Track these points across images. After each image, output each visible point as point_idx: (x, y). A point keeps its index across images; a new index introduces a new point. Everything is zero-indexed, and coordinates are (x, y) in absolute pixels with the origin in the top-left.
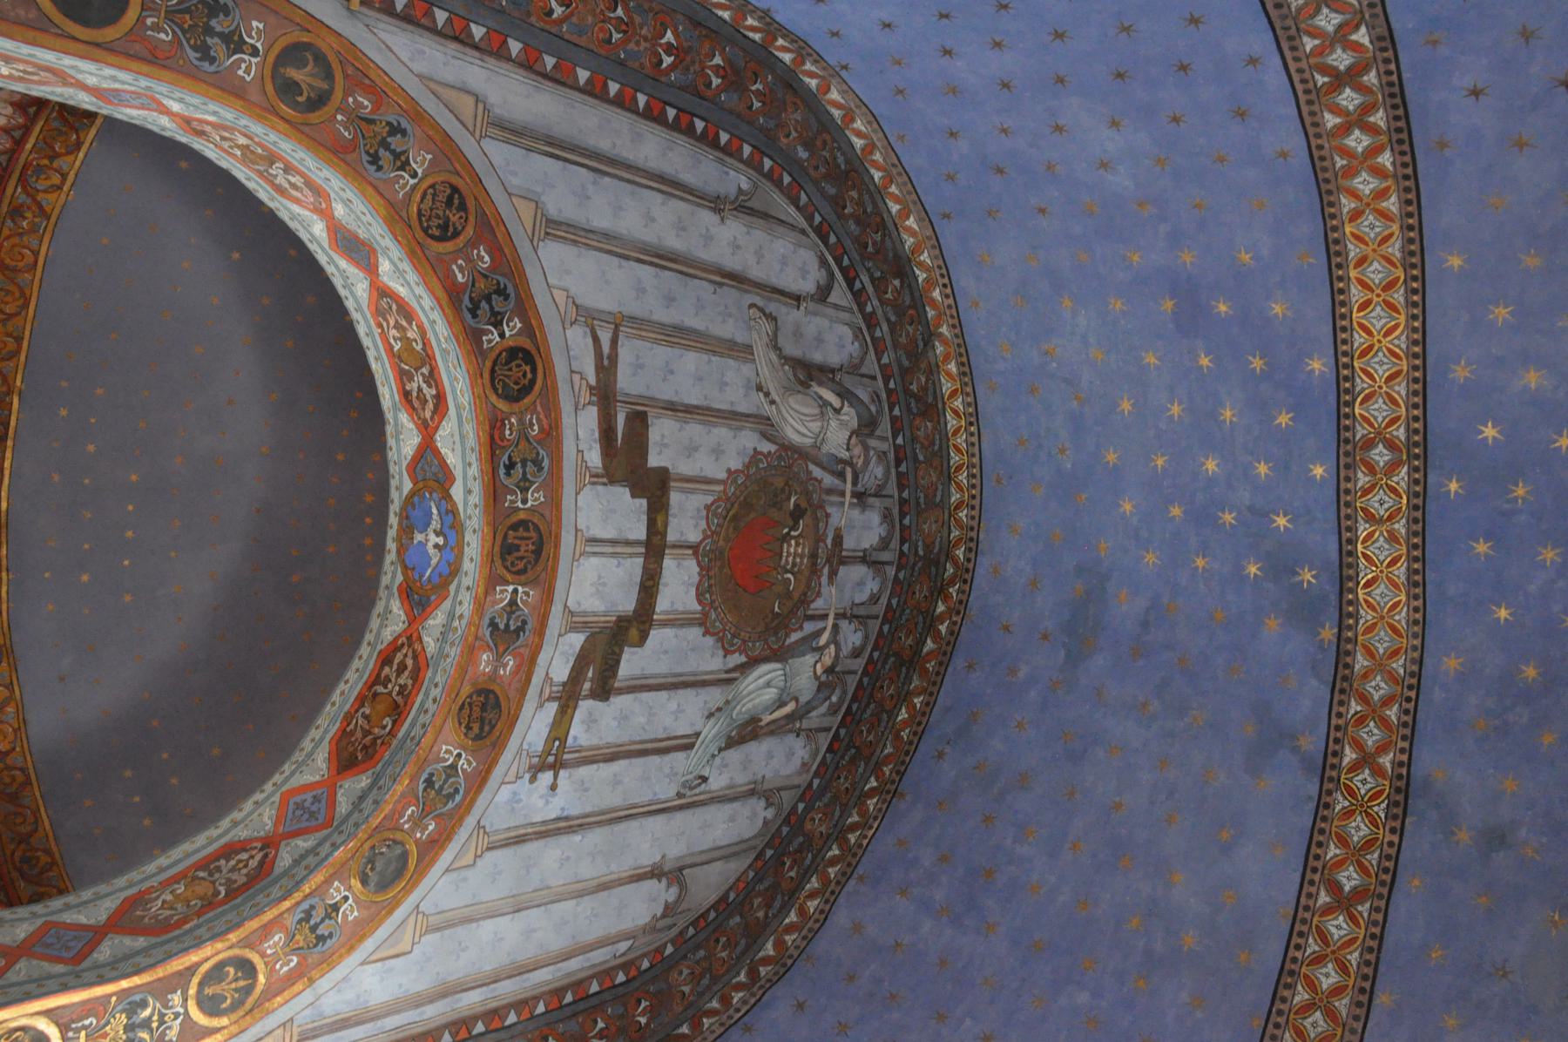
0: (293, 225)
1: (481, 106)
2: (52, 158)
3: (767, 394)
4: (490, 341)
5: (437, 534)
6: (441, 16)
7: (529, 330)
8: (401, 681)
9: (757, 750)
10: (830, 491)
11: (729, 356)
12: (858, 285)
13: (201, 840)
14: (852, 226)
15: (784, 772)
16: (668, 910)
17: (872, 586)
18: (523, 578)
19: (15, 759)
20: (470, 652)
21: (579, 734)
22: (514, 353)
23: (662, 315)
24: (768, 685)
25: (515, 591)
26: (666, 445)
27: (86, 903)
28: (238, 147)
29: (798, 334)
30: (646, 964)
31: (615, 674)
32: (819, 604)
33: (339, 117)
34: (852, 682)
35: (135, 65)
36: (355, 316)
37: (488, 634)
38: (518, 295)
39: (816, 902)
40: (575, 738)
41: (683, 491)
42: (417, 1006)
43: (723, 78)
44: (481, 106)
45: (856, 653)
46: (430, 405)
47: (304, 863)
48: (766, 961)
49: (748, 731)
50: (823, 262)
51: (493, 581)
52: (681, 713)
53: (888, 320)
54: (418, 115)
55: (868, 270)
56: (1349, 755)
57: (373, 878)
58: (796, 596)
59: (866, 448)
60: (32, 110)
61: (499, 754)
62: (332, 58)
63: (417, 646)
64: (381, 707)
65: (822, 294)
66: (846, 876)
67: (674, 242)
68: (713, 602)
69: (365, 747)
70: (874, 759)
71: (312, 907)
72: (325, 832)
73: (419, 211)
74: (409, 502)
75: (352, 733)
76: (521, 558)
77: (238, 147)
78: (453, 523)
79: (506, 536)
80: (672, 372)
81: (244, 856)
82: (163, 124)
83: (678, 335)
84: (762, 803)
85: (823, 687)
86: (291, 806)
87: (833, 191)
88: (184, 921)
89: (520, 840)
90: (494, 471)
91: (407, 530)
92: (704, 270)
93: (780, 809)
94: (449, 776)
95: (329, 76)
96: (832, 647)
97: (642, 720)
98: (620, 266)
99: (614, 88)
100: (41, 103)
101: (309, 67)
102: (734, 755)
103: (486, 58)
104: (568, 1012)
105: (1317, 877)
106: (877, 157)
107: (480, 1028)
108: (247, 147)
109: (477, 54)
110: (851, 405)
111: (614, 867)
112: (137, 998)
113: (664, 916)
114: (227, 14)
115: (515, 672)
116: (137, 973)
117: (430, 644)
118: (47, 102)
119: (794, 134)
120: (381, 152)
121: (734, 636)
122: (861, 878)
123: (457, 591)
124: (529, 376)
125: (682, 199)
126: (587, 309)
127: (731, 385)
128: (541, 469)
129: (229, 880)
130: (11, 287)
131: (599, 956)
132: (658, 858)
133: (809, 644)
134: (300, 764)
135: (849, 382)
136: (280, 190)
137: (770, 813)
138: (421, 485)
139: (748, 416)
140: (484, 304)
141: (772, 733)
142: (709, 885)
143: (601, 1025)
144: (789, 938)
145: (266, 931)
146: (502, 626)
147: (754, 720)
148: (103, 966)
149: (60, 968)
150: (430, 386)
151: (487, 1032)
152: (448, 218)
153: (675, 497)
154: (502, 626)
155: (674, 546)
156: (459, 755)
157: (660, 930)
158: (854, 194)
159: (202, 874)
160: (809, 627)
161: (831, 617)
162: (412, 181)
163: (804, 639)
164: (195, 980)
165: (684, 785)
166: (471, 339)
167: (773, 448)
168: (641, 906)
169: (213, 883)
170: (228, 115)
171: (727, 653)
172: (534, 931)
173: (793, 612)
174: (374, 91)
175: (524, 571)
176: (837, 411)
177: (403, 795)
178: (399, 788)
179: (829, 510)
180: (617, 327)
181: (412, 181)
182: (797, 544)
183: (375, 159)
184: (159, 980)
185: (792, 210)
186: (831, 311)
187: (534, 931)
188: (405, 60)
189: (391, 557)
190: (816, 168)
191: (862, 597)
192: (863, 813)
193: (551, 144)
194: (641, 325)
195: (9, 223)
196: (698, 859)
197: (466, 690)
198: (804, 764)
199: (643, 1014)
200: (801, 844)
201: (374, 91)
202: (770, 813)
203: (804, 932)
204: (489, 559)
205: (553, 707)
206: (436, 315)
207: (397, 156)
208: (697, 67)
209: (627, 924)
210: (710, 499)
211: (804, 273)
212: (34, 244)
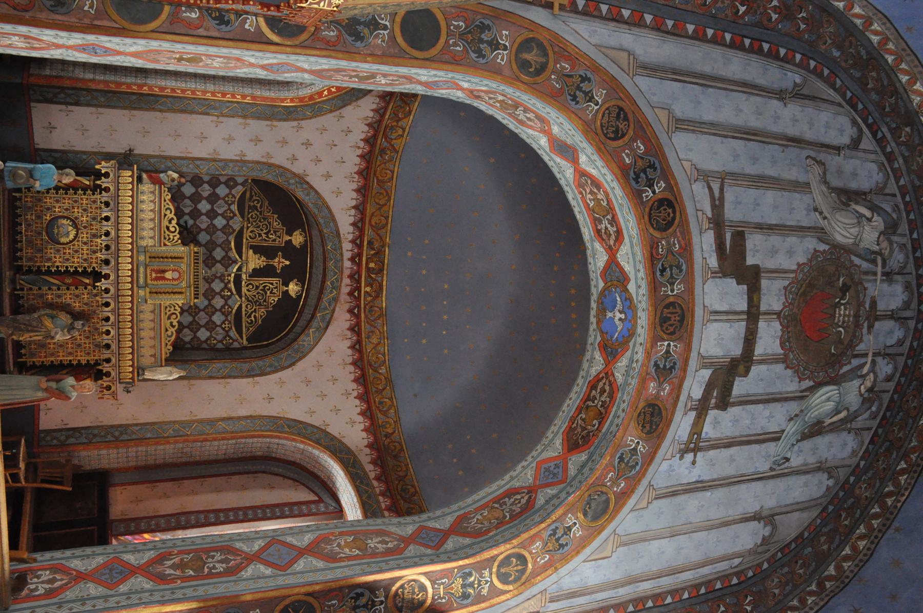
0: (528, 141)
1: (632, 57)
2: (397, 121)
3: (821, 213)
4: (647, 196)
5: (621, 312)
6: (604, 8)
8: (603, 399)
9: (821, 441)
10: (867, 273)
11: (795, 191)
12: (880, 135)
13: (494, 486)
14: (874, 96)
15: (840, 456)
16: (765, 541)
17: (899, 334)
18: (673, 337)
19: (396, 437)
20: (643, 383)
21: (708, 430)
22: (662, 202)
23: (751, 170)
24: (828, 400)
25: (669, 345)
26: (757, 251)
27: (439, 517)
28: (498, 101)
29: (840, 172)
30: (750, 574)
31: (730, 395)
32: (861, 347)
33: (553, 77)
34: (886, 398)
35: (445, 67)
36: (566, 189)
37: (653, 371)
38: (662, 168)
39: (864, 542)
40: (707, 433)
41: (769, 278)
42: (615, 588)
43: (779, 14)
44: (632, 57)
45: (889, 379)
46: (613, 237)
47: (552, 502)
48: (830, 578)
49: (816, 429)
50: (854, 123)
53: (903, 155)
54: (596, 68)
55: (887, 124)
58: (846, 342)
59: (891, 243)
60: (388, 98)
61: (661, 442)
62: (546, 44)
63: (611, 378)
64: (591, 414)
65: (855, 144)
66: (885, 527)
67: (754, 123)
68: (791, 347)
69: (583, 437)
70: (903, 450)
71: (557, 528)
72: (562, 486)
73: (601, 124)
74: (602, 294)
75: (575, 429)
76: (671, 325)
77: (498, 101)
78: (630, 306)
79: (662, 311)
80: (758, 205)
81: (518, 497)
82: (458, 95)
83: (761, 181)
84: (826, 476)
85: (866, 401)
86: (543, 470)
87: (858, 75)
88: (489, 531)
89: (674, 494)
90: (654, 273)
91: (602, 311)
92: (775, 138)
94: (633, 455)
95: (546, 55)
96: (872, 375)
97: (748, 422)
98: (722, 143)
99: (710, 32)
100: (392, 94)
101: (535, 51)
102: (807, 445)
103: (632, 28)
104: (703, 599)
106: (891, 46)
107: (650, 604)
108: (503, 101)
109: (627, 27)
110: (879, 215)
111: (731, 512)
112: (467, 571)
113: (761, 545)
114: (489, 30)
115: (670, 393)
116: (467, 558)
117: (619, 377)
118: (395, 92)
119: (829, 41)
120: (578, 93)
121: (805, 369)
122: (897, 530)
123: (634, 345)
124: (672, 215)
125: (757, 95)
126: (704, 171)
127: (796, 209)
128: (681, 271)
129: (511, 509)
130: (382, 191)
131: (722, 566)
132: (758, 508)
133: (855, 373)
134: (546, 446)
135: (877, 200)
136: (521, 122)
137: (831, 482)
138: (609, 284)
139: (809, 228)
140: (642, 175)
141: (831, 431)
142: (792, 526)
144: (846, 565)
145: (532, 539)
146: (661, 366)
147: (819, 422)
148: (451, 552)
149: (429, 551)
150: (612, 226)
151: (654, 607)
152: (618, 126)
153: (764, 283)
154: (661, 366)
155: (765, 314)
156: (638, 443)
157: (760, 553)
158: (874, 74)
159: (496, 505)
160: (855, 362)
161: (870, 355)
162: (596, 108)
163: (852, 370)
164: (496, 564)
165: (774, 463)
166: (636, 196)
167: (827, 247)
168: (747, 537)
169: (503, 510)
170: (494, 85)
171: (801, 380)
172: (682, 548)
173: (843, 354)
174: (569, 58)
175: (673, 333)
178: (605, 461)
179: (866, 285)
180: (723, 179)
181: (596, 108)
182: (845, 309)
183: (574, 98)
184: (478, 562)
185: (831, 92)
186: (861, 154)
187: (682, 548)
188: (586, 37)
189: (593, 326)
190: (846, 61)
192: (897, 484)
193: (674, 73)
194: (736, 177)
195: (379, 158)
196: (784, 510)
197: (642, 404)
198: (853, 451)
199: (748, 604)
200: (853, 503)
202: (831, 482)
203: (856, 562)
204: (653, 326)
205: (693, 415)
206: (615, 184)
207: (586, 94)
208: (762, 10)
209: (738, 548)
211: (841, 131)
212: (391, 167)
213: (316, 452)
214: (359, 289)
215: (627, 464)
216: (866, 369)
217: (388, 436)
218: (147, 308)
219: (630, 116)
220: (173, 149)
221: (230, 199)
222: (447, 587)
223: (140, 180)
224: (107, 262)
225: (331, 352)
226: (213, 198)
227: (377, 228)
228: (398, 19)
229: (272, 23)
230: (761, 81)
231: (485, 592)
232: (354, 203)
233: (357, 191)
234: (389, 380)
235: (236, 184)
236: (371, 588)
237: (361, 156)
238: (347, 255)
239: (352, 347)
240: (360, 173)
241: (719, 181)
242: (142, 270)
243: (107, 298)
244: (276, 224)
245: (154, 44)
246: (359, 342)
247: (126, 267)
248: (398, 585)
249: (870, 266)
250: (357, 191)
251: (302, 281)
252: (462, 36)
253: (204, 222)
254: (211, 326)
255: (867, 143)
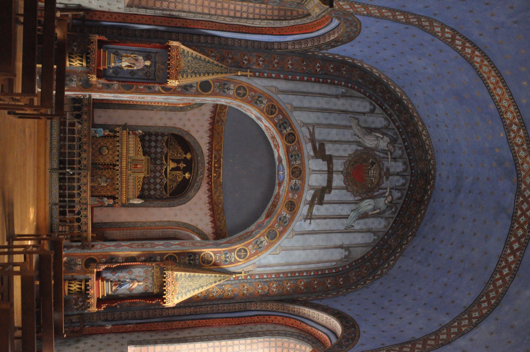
3: (358, 136)
7: (292, 129)
10: (383, 158)
12: (384, 108)
16: (346, 257)
17: (402, 181)
21: (315, 212)
22: (290, 134)
23: (325, 122)
24: (369, 205)
26: (329, 150)
29: (366, 121)
32: (383, 186)
34: (399, 207)
45: (399, 198)
49: (364, 216)
50: (371, 104)
51: (290, 179)
52: (345, 210)
54: (264, 93)
56: (519, 212)
57: (270, 237)
59: (394, 147)
62: (246, 88)
65: (372, 111)
67: (326, 106)
89: (303, 234)
93: (378, 237)
102: (362, 221)
105: (508, 246)
111: (329, 244)
127: (348, 135)
131: (327, 264)
133: (382, 195)
137: (376, 237)
142: (358, 253)
143: (329, 281)
152: (271, 109)
153: (334, 161)
158: (379, 86)
164: (236, 251)
166: (280, 132)
167: (362, 148)
168: (338, 255)
171: (355, 196)
176: (382, 138)
177: (275, 221)
180: (314, 126)
183: (256, 103)
185: (359, 94)
191: (400, 184)
194: (320, 125)
197: (287, 201)
198: (385, 226)
199: (341, 281)
201: (255, 91)
205: (308, 206)
210: (345, 161)
213: (193, 235)
214: (211, 174)
215: (283, 221)
216: (387, 195)
217: (221, 230)
218: (131, 178)
219: (277, 107)
220: (141, 123)
221: (162, 141)
222: (220, 257)
223: (129, 133)
224: (118, 161)
225: (200, 199)
226: (156, 141)
227: (219, 151)
228: (199, 84)
229: (163, 88)
230: (328, 92)
231: (233, 260)
232: (208, 141)
233: (209, 137)
234: (223, 209)
235: (165, 135)
236: (195, 254)
237: (210, 124)
238: (206, 161)
239: (209, 197)
240: (209, 130)
241: (312, 127)
242: (129, 164)
243: (118, 172)
244: (180, 150)
245: (132, 95)
246: (211, 195)
247: (124, 163)
248: (203, 254)
249: (385, 156)
250: (209, 137)
251: (190, 173)
252: (218, 87)
253: (153, 150)
254: (155, 189)
255: (378, 110)
